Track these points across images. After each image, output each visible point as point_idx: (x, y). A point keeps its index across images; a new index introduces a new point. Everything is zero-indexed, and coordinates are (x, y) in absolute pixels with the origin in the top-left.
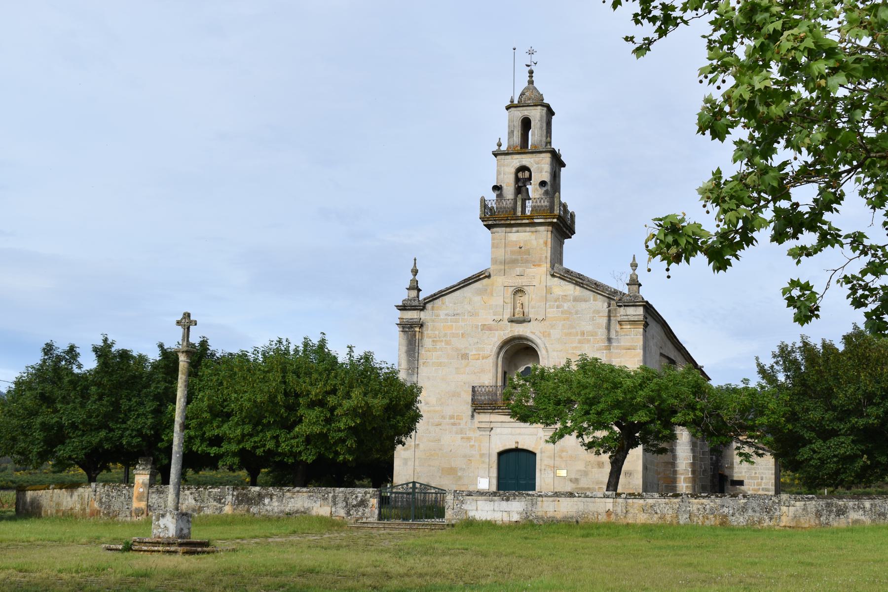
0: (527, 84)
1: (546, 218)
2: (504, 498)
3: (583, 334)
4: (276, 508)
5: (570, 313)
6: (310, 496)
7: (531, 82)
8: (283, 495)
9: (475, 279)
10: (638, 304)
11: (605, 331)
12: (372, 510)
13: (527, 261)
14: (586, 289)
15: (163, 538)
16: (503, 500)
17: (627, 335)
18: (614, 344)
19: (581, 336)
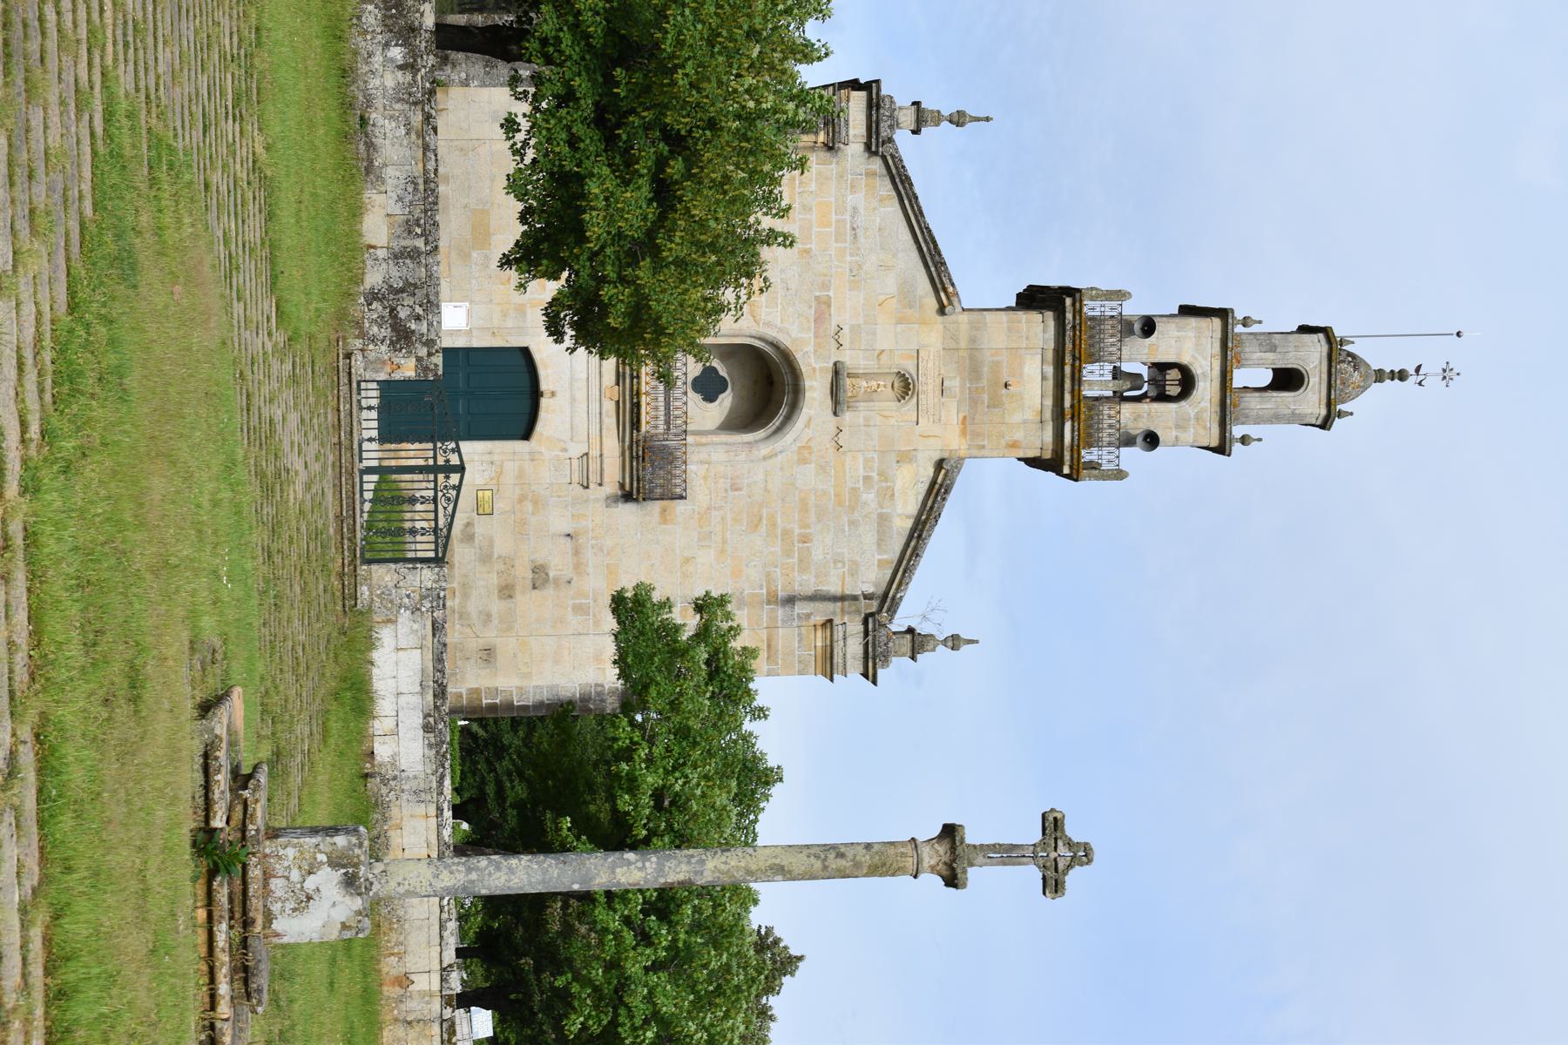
0: (1375, 367)
1: (1072, 450)
2: (431, 720)
3: (805, 539)
4: (377, 82)
5: (852, 509)
6: (416, 184)
7: (1380, 376)
8: (415, 104)
9: (937, 280)
10: (870, 665)
11: (810, 589)
12: (384, 362)
13: (974, 402)
14: (907, 545)
15: (266, 891)
16: (426, 716)
17: (800, 642)
18: (780, 612)
19: (799, 535)
